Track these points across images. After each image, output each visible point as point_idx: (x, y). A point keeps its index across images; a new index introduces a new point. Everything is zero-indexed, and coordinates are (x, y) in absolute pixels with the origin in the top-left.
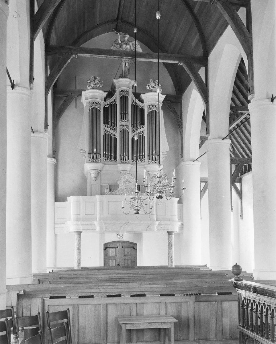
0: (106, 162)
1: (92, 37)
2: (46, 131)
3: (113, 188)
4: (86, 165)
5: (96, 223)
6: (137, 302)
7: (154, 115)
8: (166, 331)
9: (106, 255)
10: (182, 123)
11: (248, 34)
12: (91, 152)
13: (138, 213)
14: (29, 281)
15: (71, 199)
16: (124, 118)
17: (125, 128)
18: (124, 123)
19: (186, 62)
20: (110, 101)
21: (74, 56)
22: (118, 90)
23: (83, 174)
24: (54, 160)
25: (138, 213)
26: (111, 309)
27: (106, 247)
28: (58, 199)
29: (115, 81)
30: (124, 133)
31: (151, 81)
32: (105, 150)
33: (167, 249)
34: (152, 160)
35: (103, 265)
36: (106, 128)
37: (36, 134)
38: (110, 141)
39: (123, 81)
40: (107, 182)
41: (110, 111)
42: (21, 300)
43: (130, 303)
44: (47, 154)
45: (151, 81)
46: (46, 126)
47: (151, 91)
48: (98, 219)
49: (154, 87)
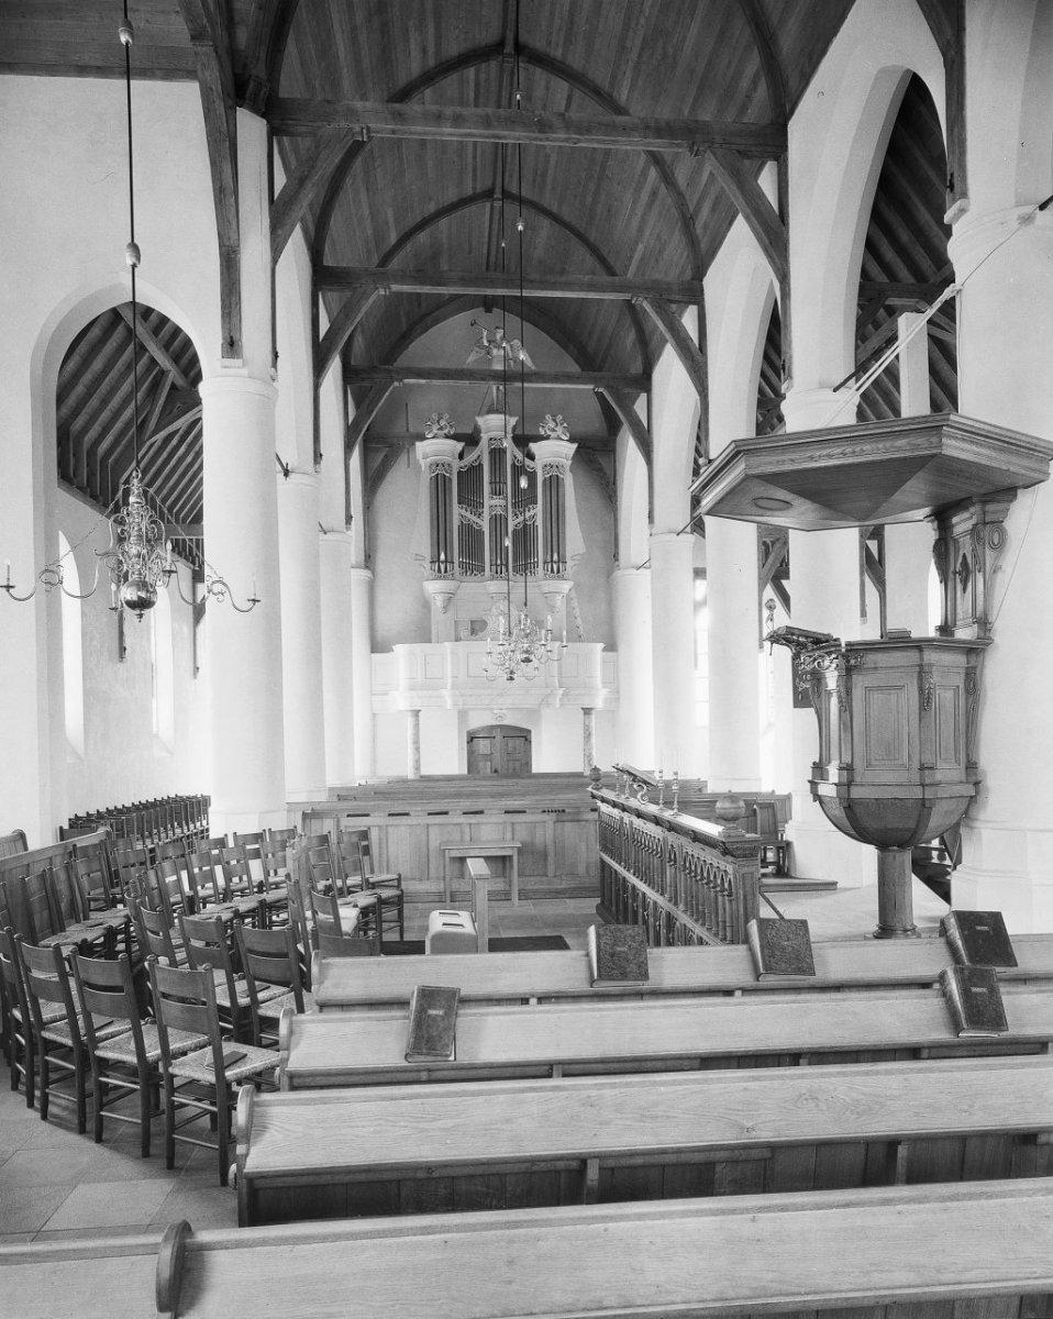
0: (464, 578)
1: (437, 321)
2: (348, 529)
3: (477, 628)
4: (426, 584)
5: (446, 693)
6: (471, 821)
7: (554, 484)
8: (510, 857)
9: (471, 753)
10: (615, 492)
11: (699, 357)
12: (435, 560)
13: (512, 679)
14: (322, 797)
15: (400, 650)
16: (496, 492)
17: (499, 511)
18: (498, 501)
19: (606, 387)
20: (470, 458)
21: (396, 384)
22: (485, 437)
23: (424, 598)
24: (365, 574)
25: (512, 679)
26: (434, 832)
27: (471, 738)
28: (377, 646)
29: (480, 421)
30: (498, 522)
31: (548, 417)
32: (461, 553)
33: (581, 739)
34: (552, 571)
35: (466, 772)
36: (463, 512)
37: (329, 536)
38: (471, 536)
39: (635, 202)
40: (465, 616)
41: (470, 478)
42: (308, 821)
43: (460, 824)
44: (353, 560)
45: (548, 417)
46: (349, 519)
47: (548, 438)
48: (449, 685)
49: (554, 430)
